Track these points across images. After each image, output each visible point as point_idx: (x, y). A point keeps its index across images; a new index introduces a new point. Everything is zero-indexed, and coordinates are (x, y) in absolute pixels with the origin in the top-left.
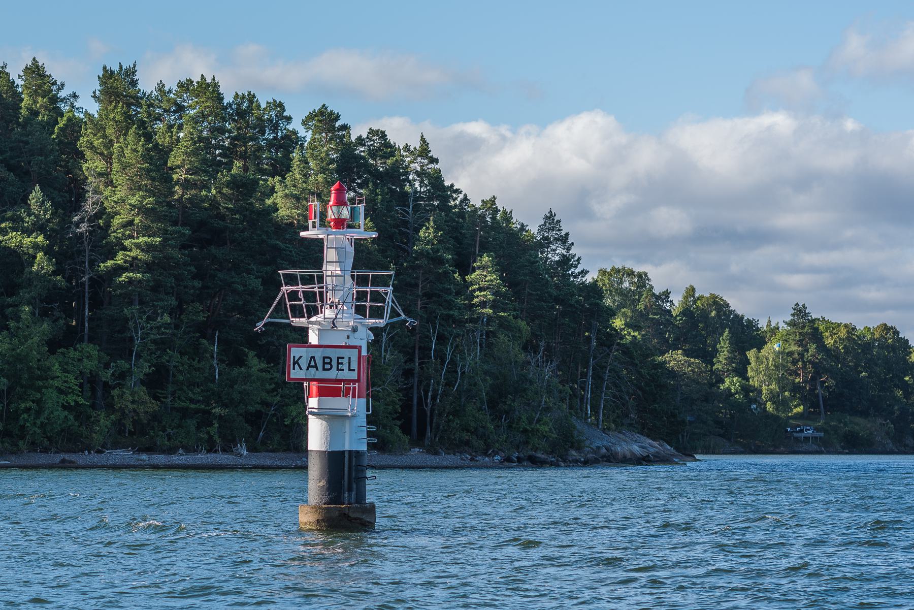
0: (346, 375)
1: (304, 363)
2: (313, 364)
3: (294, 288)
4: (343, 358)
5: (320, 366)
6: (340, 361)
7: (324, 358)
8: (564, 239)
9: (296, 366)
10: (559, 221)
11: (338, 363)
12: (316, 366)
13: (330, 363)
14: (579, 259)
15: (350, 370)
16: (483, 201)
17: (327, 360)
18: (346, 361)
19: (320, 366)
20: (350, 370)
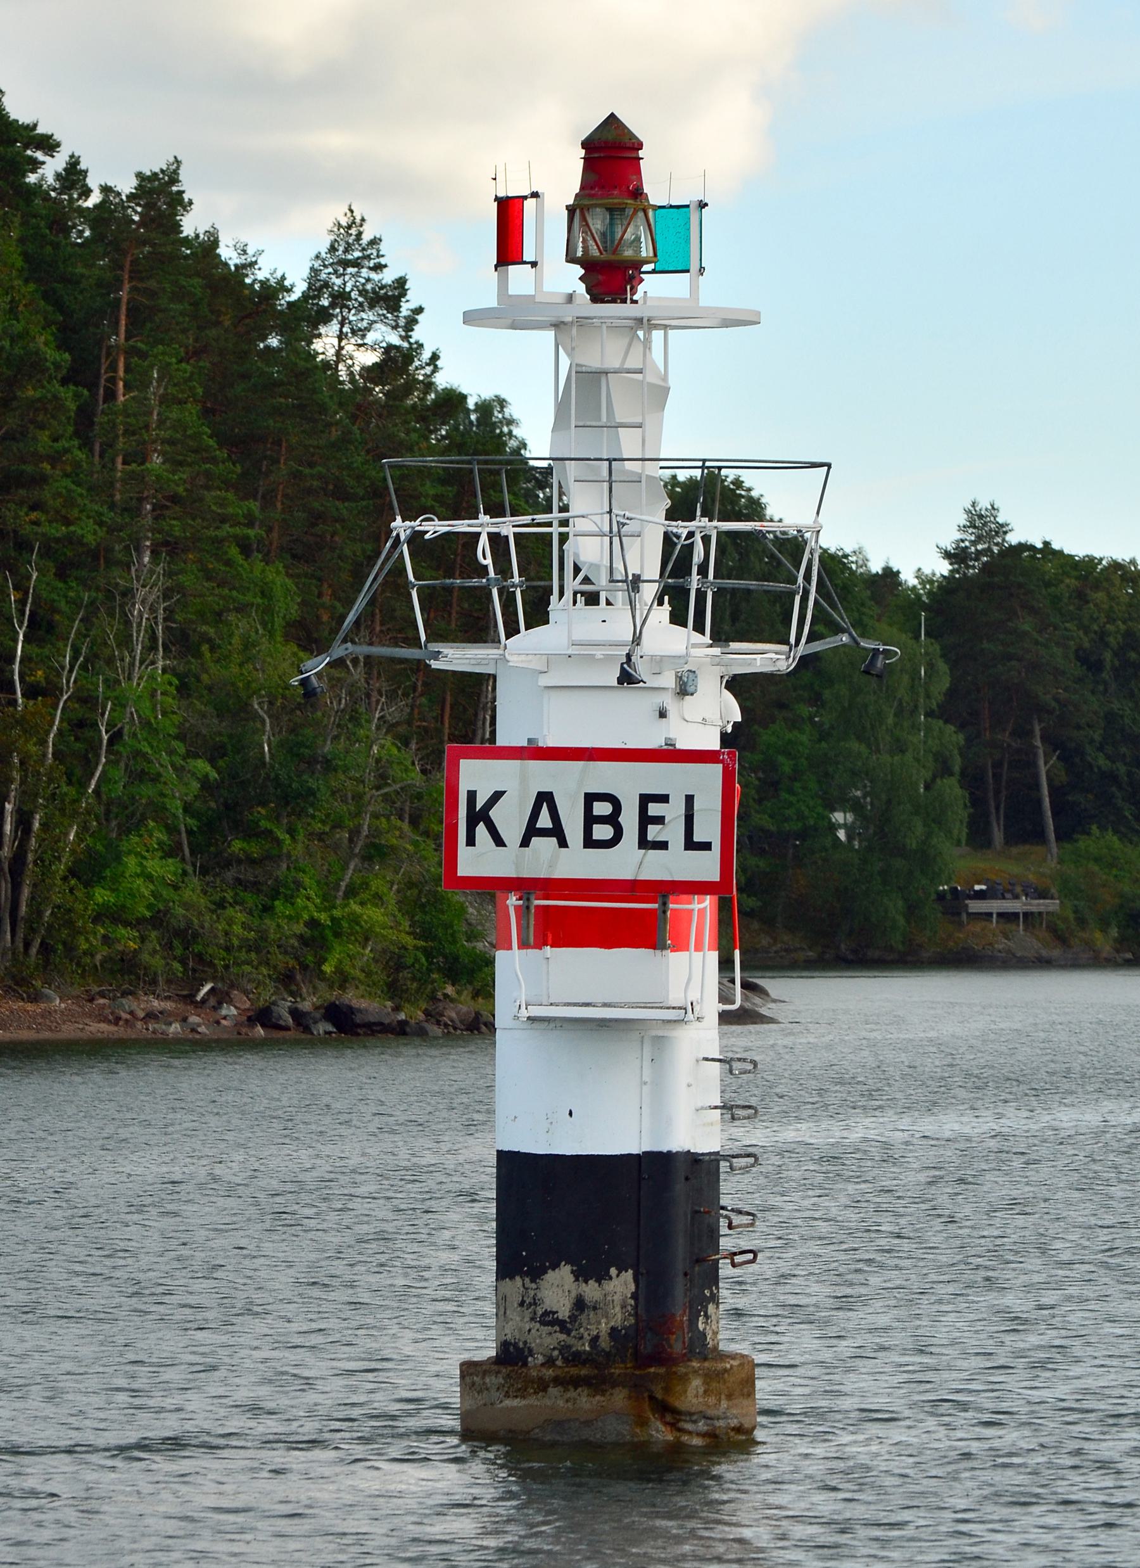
0: (675, 864)
1: (510, 818)
2: (544, 821)
3: (462, 526)
4: (664, 799)
5: (574, 828)
6: (654, 809)
7: (590, 799)
8: (389, 298)
9: (481, 829)
10: (375, 242)
11: (645, 819)
12: (557, 832)
13: (613, 820)
14: (435, 357)
15: (691, 844)
16: (139, 175)
17: (602, 809)
18: (673, 811)
19: (574, 828)
20: (691, 844)
